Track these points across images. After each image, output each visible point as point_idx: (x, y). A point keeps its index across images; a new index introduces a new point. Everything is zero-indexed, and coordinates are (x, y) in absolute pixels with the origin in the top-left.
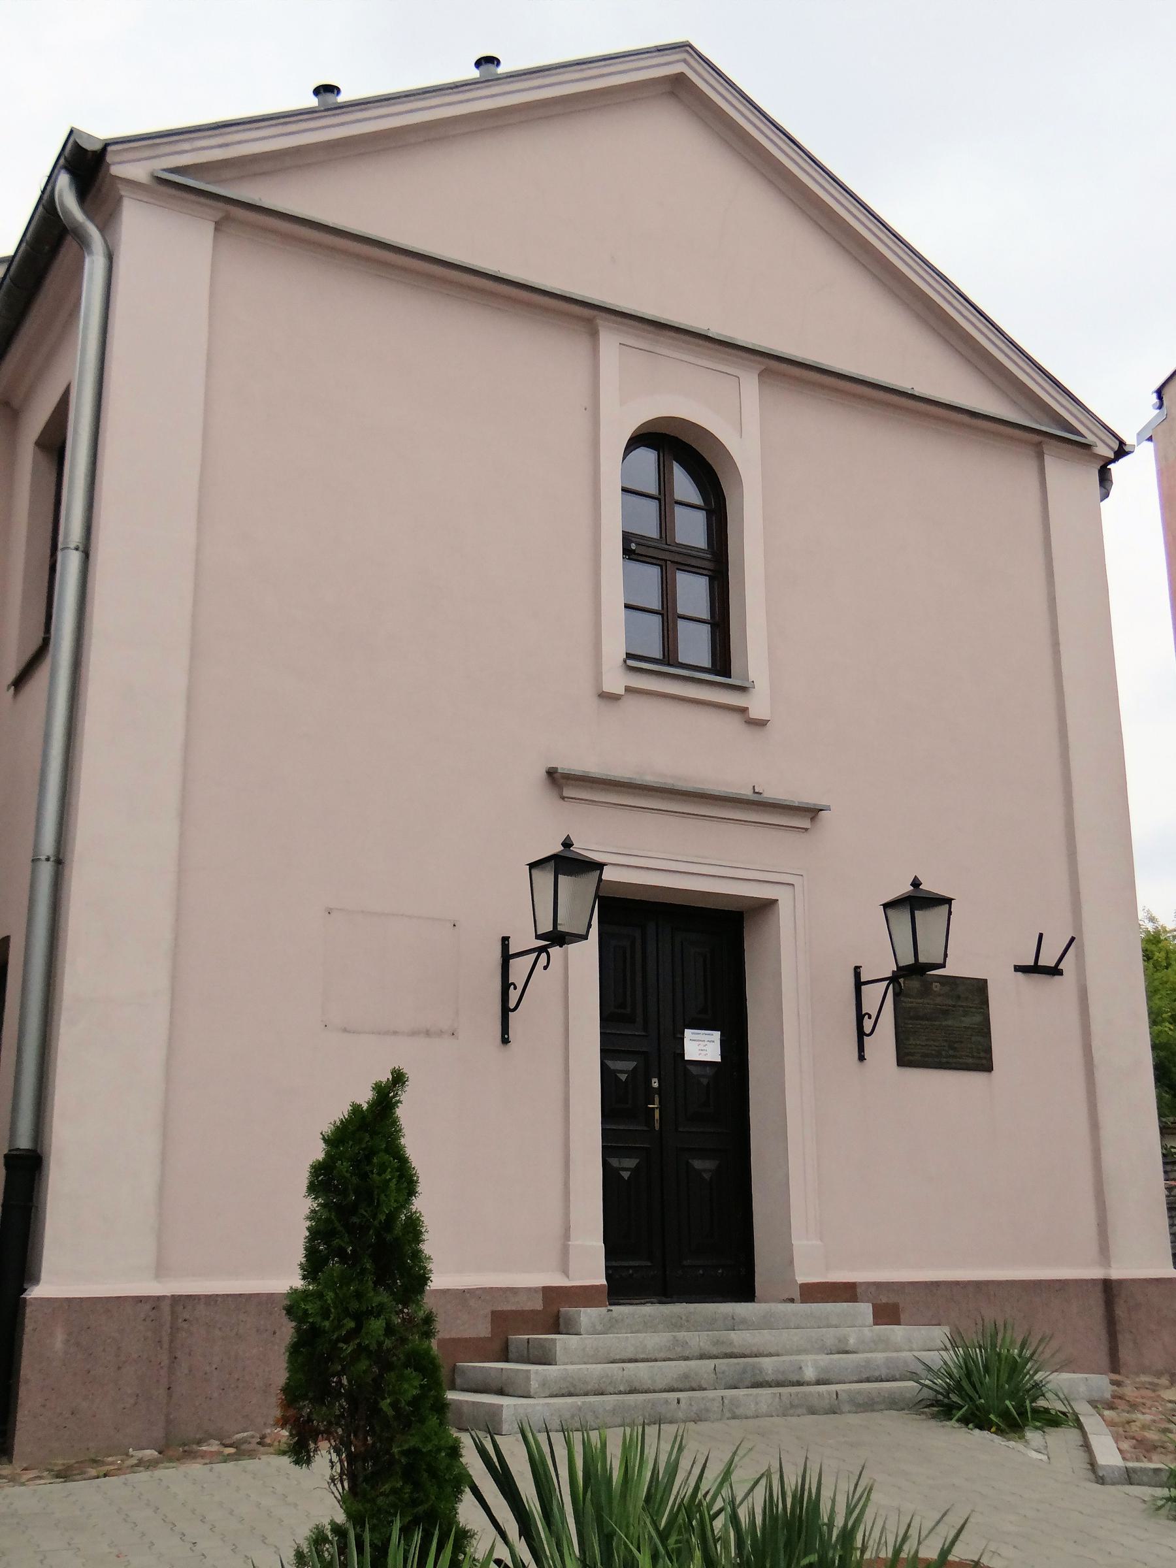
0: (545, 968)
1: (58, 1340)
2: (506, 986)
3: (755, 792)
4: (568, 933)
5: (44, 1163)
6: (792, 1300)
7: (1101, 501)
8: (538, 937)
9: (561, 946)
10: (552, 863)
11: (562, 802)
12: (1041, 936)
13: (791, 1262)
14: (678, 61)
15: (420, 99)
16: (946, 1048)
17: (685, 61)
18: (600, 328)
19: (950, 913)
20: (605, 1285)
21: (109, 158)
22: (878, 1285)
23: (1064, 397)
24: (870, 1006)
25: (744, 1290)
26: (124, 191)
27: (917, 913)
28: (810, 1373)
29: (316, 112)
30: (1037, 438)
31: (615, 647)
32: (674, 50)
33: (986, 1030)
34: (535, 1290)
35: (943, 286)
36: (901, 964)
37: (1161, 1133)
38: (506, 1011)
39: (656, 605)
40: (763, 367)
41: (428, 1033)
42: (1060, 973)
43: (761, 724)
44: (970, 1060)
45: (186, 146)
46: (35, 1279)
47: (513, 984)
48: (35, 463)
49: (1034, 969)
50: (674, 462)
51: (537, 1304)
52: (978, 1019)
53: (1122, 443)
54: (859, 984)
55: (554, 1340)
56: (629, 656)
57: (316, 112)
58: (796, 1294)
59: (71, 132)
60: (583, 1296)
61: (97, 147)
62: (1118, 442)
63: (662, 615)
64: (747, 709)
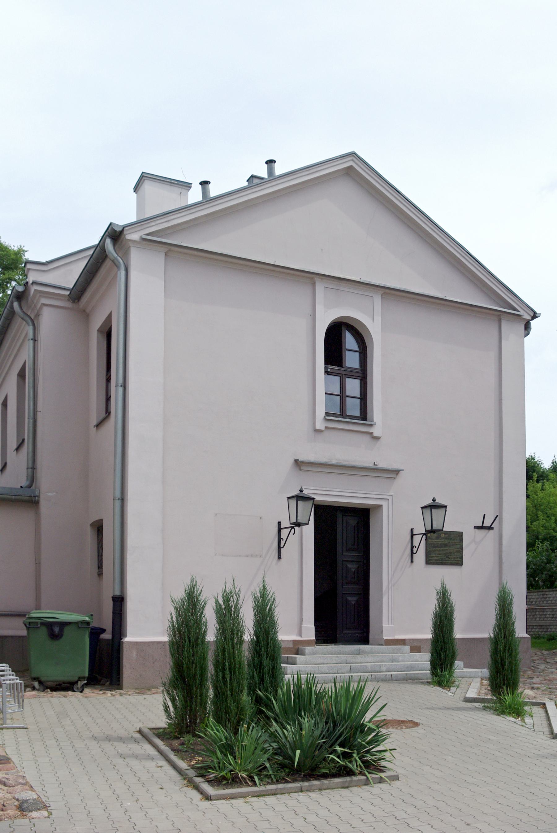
0: (293, 534)
1: (134, 654)
2: (280, 539)
3: (375, 465)
4: (301, 523)
5: (125, 599)
6: (382, 645)
7: (525, 337)
8: (291, 524)
9: (299, 527)
10: (296, 498)
11: (300, 472)
12: (484, 515)
13: (382, 632)
14: (350, 160)
15: (243, 192)
16: (445, 558)
17: (352, 160)
18: (316, 281)
19: (446, 511)
20: (314, 640)
21: (125, 232)
22: (414, 640)
23: (512, 295)
24: (416, 543)
25: (365, 640)
26: (131, 244)
27: (433, 510)
28: (384, 669)
29: (202, 203)
30: (499, 313)
31: (321, 412)
32: (348, 156)
33: (461, 551)
34: (291, 641)
35: (461, 250)
36: (427, 529)
37: (528, 589)
38: (279, 548)
39: (338, 392)
40: (383, 292)
41: (252, 556)
42: (493, 529)
43: (378, 438)
44: (454, 562)
45: (153, 224)
46: (126, 636)
47: (282, 538)
48: (98, 339)
49: (482, 527)
50: (346, 331)
51: (291, 646)
52: (458, 546)
53: (535, 313)
54: (412, 536)
55: (296, 657)
56: (327, 414)
57: (202, 203)
58: (384, 643)
59: (111, 224)
60: (308, 643)
61: (120, 229)
62: (533, 313)
63: (340, 396)
64: (373, 433)
